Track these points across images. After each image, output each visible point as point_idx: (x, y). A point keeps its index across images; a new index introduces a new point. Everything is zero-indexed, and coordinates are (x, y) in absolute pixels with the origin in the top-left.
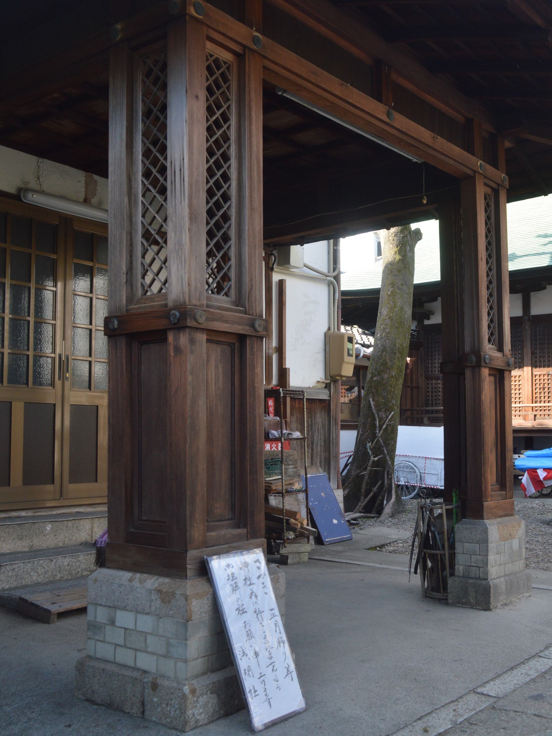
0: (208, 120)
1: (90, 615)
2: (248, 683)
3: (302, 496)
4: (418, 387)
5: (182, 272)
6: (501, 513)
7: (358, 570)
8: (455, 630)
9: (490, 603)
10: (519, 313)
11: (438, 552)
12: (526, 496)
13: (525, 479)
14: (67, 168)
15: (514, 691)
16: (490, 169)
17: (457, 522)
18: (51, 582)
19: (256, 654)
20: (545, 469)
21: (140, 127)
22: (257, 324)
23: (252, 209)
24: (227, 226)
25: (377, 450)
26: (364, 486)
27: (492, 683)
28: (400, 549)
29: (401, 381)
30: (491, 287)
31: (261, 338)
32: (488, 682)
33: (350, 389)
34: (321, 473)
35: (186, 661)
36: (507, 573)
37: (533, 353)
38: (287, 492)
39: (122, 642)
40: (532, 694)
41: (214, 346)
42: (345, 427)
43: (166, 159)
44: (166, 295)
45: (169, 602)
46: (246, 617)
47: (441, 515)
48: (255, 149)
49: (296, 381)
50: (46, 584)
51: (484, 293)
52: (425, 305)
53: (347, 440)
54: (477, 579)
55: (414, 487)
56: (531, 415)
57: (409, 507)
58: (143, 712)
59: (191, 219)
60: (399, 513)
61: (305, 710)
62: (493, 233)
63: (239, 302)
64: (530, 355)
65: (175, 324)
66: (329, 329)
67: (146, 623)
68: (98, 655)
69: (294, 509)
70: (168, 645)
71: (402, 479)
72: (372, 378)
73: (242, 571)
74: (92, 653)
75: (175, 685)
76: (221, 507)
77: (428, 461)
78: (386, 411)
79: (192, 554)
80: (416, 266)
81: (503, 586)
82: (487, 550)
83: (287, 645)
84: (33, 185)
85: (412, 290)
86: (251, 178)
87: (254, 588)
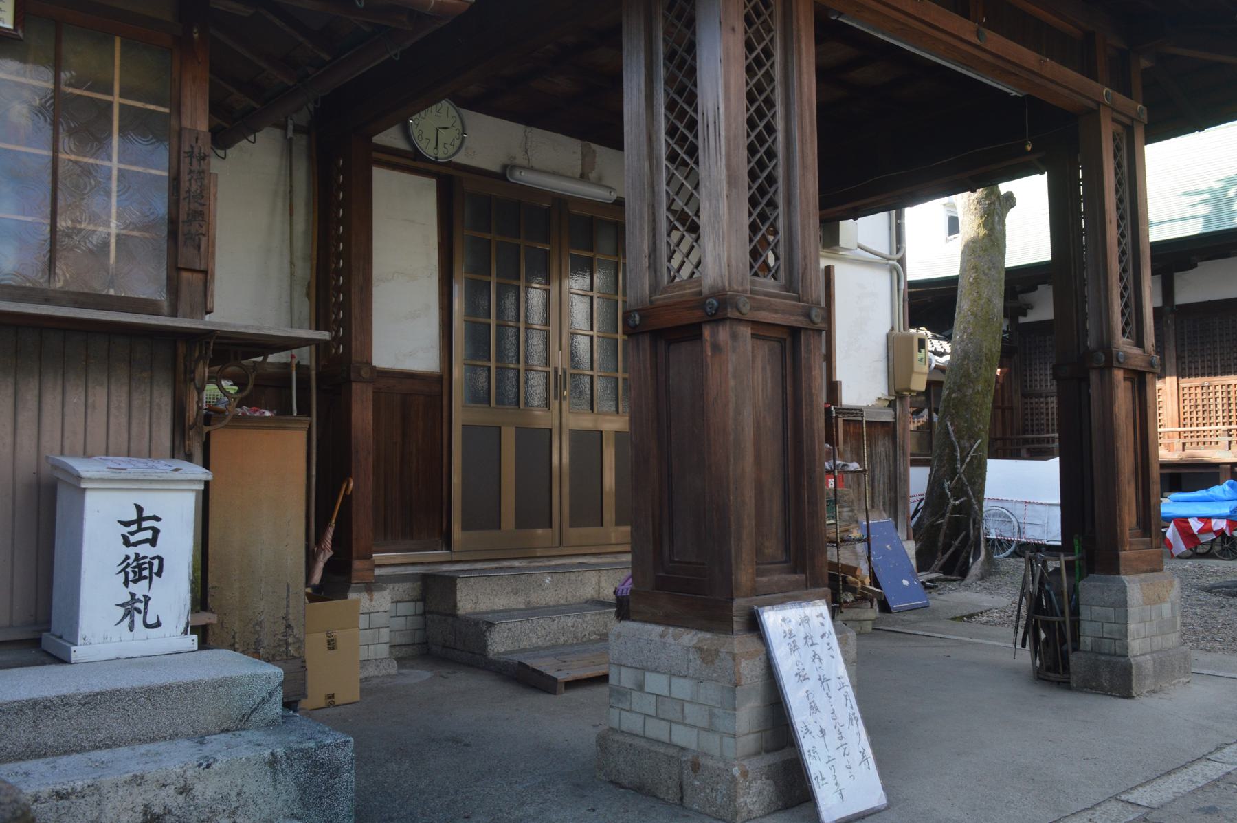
0: (747, 58)
1: (612, 681)
2: (815, 767)
3: (861, 548)
4: (1011, 408)
5: (720, 253)
6: (1145, 568)
7: (942, 643)
8: (1077, 729)
9: (1131, 688)
10: (1159, 303)
11: (1055, 618)
12: (1172, 556)
13: (1171, 532)
14: (560, 137)
15: (1174, 801)
16: (1120, 98)
17: (1081, 578)
18: (553, 646)
19: (823, 732)
20: (1200, 518)
21: (661, 73)
22: (814, 313)
23: (804, 167)
24: (773, 190)
25: (959, 491)
26: (941, 538)
27: (1140, 789)
28: (997, 620)
29: (990, 398)
30: (1124, 259)
31: (819, 331)
32: (1135, 788)
33: (917, 413)
34: (886, 519)
35: (734, 736)
36: (1155, 649)
37: (1178, 358)
38: (843, 541)
39: (653, 712)
40: (1201, 806)
41: (760, 342)
42: (916, 463)
43: (695, 111)
44: (699, 280)
45: (712, 662)
46: (808, 685)
47: (1057, 571)
48: (806, 89)
49: (848, 398)
50: (547, 648)
51: (1114, 267)
52: (1020, 296)
53: (918, 479)
54: (1110, 654)
55: (1010, 542)
56: (1177, 444)
57: (1004, 568)
58: (682, 799)
59: (729, 183)
60: (991, 575)
61: (887, 808)
62: (1126, 185)
63: (790, 286)
64: (1174, 360)
65: (712, 315)
66: (893, 329)
67: (682, 688)
68: (624, 728)
69: (852, 563)
70: (712, 715)
71: (992, 531)
72: (949, 395)
73: (802, 628)
74: (616, 726)
75: (721, 765)
76: (773, 547)
77: (1029, 506)
78: (970, 438)
79: (739, 603)
80: (1008, 242)
81: (1150, 666)
82: (1126, 617)
83: (860, 722)
84: (520, 160)
85: (1003, 275)
86: (802, 128)
87: (817, 649)
